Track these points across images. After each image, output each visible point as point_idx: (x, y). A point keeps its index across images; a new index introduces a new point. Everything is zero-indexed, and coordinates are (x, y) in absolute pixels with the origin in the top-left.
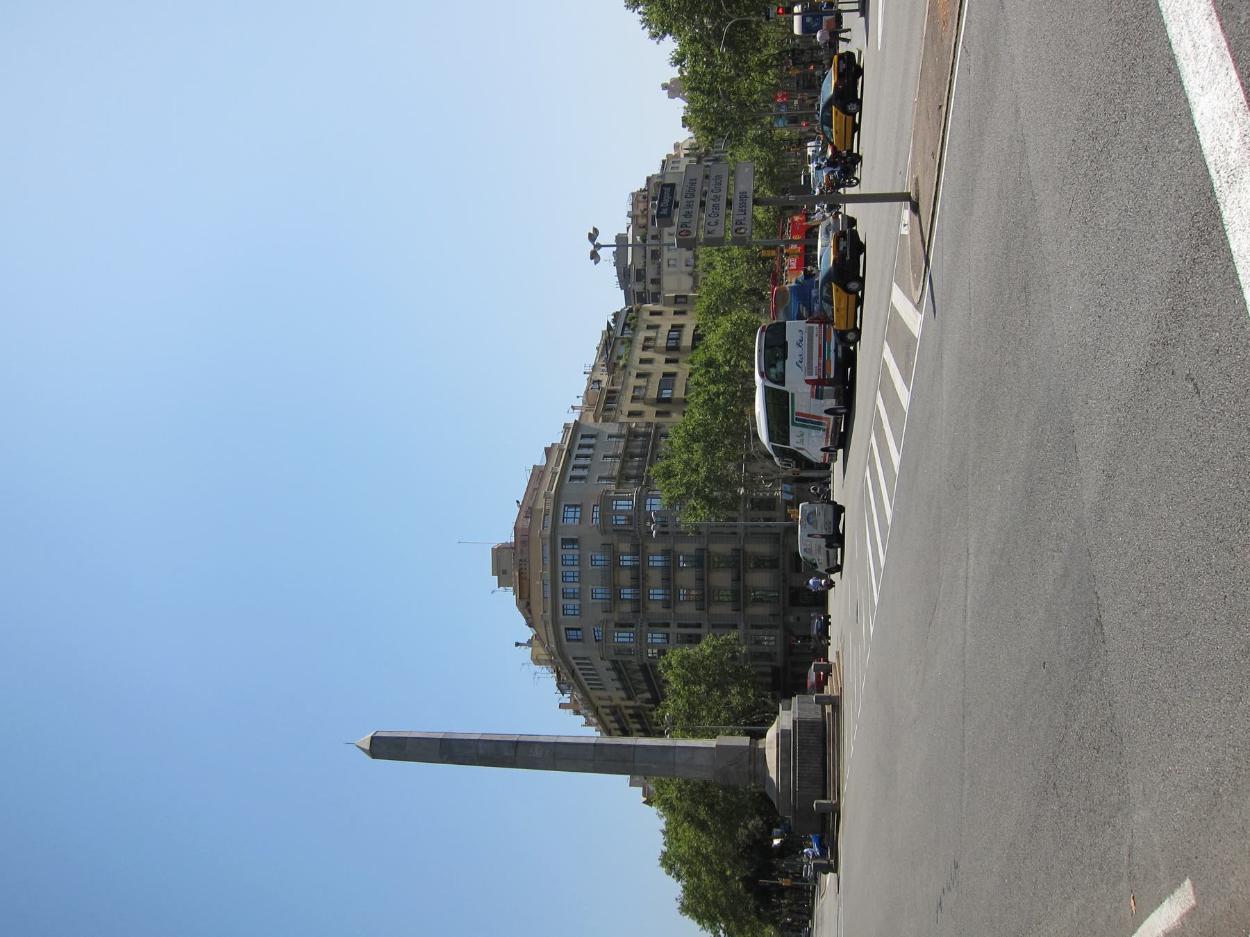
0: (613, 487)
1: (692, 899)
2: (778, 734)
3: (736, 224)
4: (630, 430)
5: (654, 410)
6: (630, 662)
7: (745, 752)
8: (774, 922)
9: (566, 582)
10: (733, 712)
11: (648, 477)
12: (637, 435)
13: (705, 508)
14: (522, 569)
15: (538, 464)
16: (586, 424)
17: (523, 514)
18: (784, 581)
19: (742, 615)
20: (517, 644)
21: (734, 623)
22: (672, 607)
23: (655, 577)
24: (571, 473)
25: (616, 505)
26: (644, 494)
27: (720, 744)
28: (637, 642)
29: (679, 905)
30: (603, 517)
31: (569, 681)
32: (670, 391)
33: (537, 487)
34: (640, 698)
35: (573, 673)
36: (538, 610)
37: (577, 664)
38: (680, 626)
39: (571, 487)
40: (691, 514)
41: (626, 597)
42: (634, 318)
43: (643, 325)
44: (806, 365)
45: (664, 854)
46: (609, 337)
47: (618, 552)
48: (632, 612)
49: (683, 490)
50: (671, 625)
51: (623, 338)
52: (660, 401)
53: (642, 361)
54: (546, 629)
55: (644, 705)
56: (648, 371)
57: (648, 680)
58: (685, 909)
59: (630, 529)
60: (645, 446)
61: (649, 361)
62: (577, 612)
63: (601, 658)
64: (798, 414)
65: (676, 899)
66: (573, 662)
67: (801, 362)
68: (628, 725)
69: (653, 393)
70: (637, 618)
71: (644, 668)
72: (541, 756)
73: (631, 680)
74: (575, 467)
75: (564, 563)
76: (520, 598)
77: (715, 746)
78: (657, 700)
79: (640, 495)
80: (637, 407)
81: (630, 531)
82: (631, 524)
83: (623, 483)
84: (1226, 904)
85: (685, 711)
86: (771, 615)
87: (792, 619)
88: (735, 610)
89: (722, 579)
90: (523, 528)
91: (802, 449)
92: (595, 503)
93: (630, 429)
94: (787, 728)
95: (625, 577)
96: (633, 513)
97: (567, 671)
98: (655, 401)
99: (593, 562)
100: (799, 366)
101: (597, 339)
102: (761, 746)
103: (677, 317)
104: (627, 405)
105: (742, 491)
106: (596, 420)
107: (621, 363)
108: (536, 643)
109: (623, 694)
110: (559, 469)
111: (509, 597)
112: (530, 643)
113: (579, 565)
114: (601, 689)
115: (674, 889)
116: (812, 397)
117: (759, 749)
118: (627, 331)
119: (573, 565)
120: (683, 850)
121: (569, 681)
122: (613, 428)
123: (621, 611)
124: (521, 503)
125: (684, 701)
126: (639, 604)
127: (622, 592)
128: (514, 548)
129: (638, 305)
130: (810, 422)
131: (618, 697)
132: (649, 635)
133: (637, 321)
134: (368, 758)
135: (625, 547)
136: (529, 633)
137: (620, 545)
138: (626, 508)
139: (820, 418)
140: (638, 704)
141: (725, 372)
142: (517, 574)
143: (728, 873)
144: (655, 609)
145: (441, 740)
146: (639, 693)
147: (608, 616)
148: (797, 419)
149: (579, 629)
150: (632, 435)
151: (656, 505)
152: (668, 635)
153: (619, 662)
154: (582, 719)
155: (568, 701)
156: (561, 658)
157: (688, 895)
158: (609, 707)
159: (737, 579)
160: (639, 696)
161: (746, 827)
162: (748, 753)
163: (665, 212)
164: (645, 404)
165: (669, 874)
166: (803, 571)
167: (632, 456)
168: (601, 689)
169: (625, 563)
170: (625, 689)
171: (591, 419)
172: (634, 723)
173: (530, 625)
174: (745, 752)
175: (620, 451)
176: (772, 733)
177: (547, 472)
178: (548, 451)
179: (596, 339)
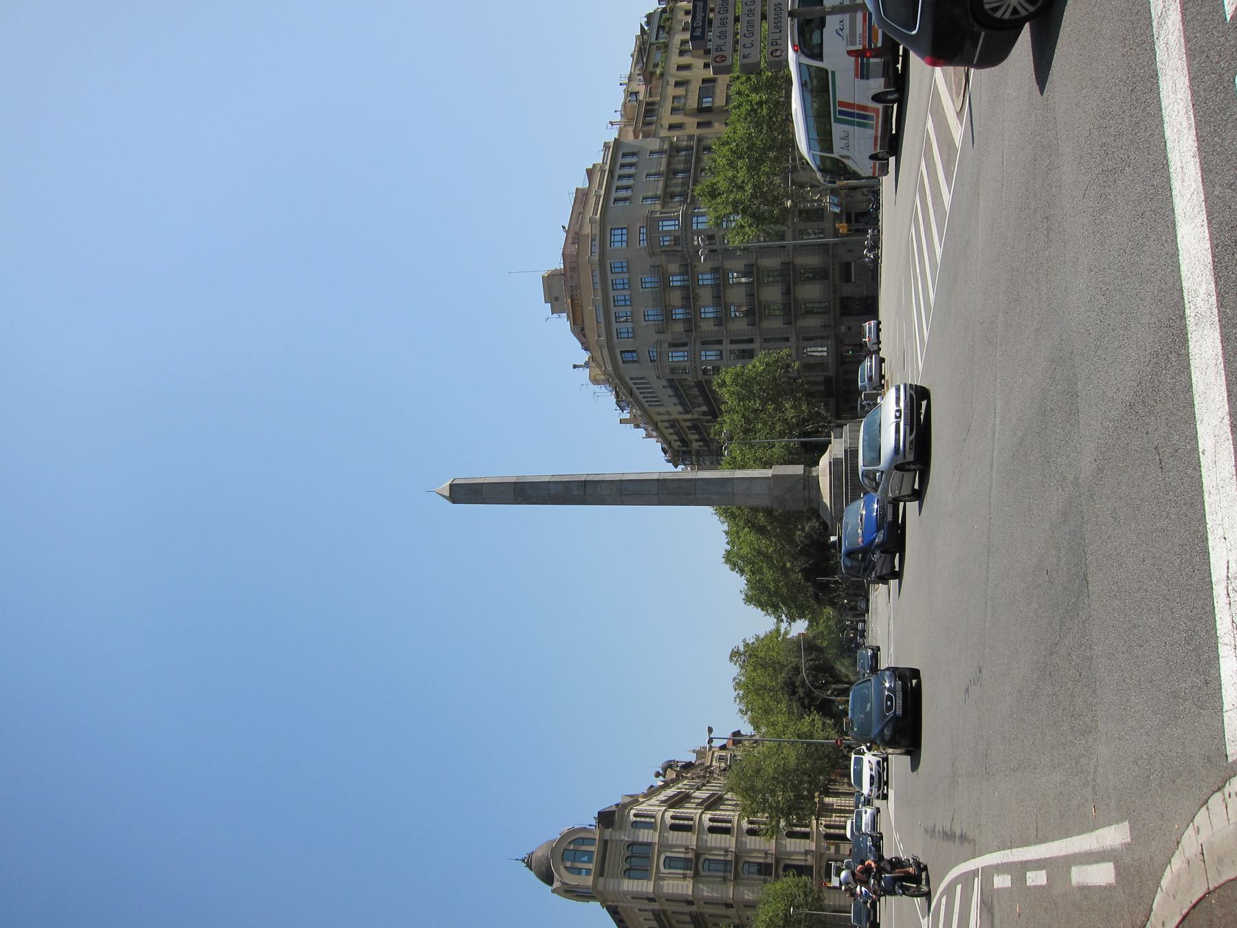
0: (658, 207)
1: (756, 590)
2: (830, 463)
3: (772, 45)
4: (671, 145)
5: (695, 121)
6: (686, 379)
7: (800, 480)
8: (833, 604)
9: (616, 289)
10: (788, 424)
11: (693, 196)
12: (679, 150)
13: (752, 226)
14: (573, 295)
15: (580, 187)
16: (626, 141)
17: (570, 241)
18: (834, 292)
19: (794, 328)
20: (575, 367)
21: (786, 336)
22: (724, 324)
23: (706, 296)
24: (614, 195)
25: (663, 226)
26: (689, 212)
27: (775, 473)
28: (691, 361)
29: (743, 596)
30: (650, 239)
31: (628, 400)
32: (710, 99)
33: (582, 211)
34: (696, 412)
35: (631, 393)
36: (592, 337)
37: (634, 384)
38: (732, 342)
39: (617, 210)
40: (738, 233)
41: (678, 317)
42: (668, 19)
43: (678, 27)
44: (848, 33)
45: (728, 552)
46: (643, 43)
47: (667, 273)
48: (685, 331)
49: (730, 209)
50: (724, 342)
51: (658, 43)
52: (701, 110)
53: (680, 68)
54: (602, 353)
55: (702, 417)
56: (688, 78)
58: (749, 599)
59: (677, 249)
60: (688, 161)
61: (687, 67)
62: (631, 335)
63: (657, 378)
64: (841, 104)
65: (741, 591)
66: (631, 383)
67: (842, 30)
68: (687, 436)
69: (693, 103)
70: (690, 337)
71: (699, 384)
72: (608, 493)
73: (687, 395)
74: (618, 188)
75: (615, 288)
76: (574, 324)
77: (770, 476)
78: (714, 413)
79: (686, 214)
80: (677, 119)
81: (677, 251)
82: (675, 244)
83: (668, 203)
85: (741, 425)
86: (822, 326)
87: (843, 329)
88: (787, 324)
89: (772, 294)
90: (570, 255)
91: (848, 158)
92: (642, 225)
93: (671, 144)
94: (839, 457)
95: (676, 298)
96: (679, 233)
97: (625, 391)
98: (696, 111)
99: (644, 285)
100: (839, 34)
101: (631, 46)
102: (814, 474)
104: (667, 118)
105: (789, 203)
106: (636, 136)
107: (658, 71)
108: (593, 364)
109: (680, 409)
110: (603, 192)
111: (563, 323)
112: (587, 365)
113: (631, 305)
114: (659, 405)
115: (739, 583)
116: (856, 76)
117: (812, 477)
118: (663, 34)
119: (622, 272)
120: (746, 550)
121: (628, 400)
122: (654, 144)
123: (674, 330)
124: (567, 229)
125: (740, 415)
126: (691, 323)
127: (673, 312)
128: (564, 275)
129: (671, 4)
130: (855, 115)
131: (676, 411)
132: (703, 353)
133: (671, 23)
134: (449, 503)
135: (674, 267)
136: (584, 356)
137: (669, 265)
138: (672, 228)
139: (865, 108)
140: (696, 416)
141: (767, 76)
142: (569, 301)
143: (788, 565)
144: (708, 327)
145: (515, 483)
146: (695, 407)
147: (662, 337)
148: (841, 113)
149: (634, 351)
150: (675, 149)
151: (704, 222)
152: (721, 351)
153: (676, 380)
154: (642, 432)
155: (628, 416)
156: (619, 379)
157: (752, 588)
158: (668, 421)
159: (788, 292)
160: (696, 409)
161: (803, 529)
162: (802, 481)
163: (698, 33)
164: (685, 115)
165: (733, 570)
166: (853, 280)
167: (676, 173)
168: (659, 405)
169: (675, 284)
170: (682, 404)
171: (631, 136)
172: (692, 434)
173: (586, 349)
174: (800, 480)
175: (663, 168)
176: (825, 461)
177: (591, 195)
178: (590, 173)
179: (630, 46)
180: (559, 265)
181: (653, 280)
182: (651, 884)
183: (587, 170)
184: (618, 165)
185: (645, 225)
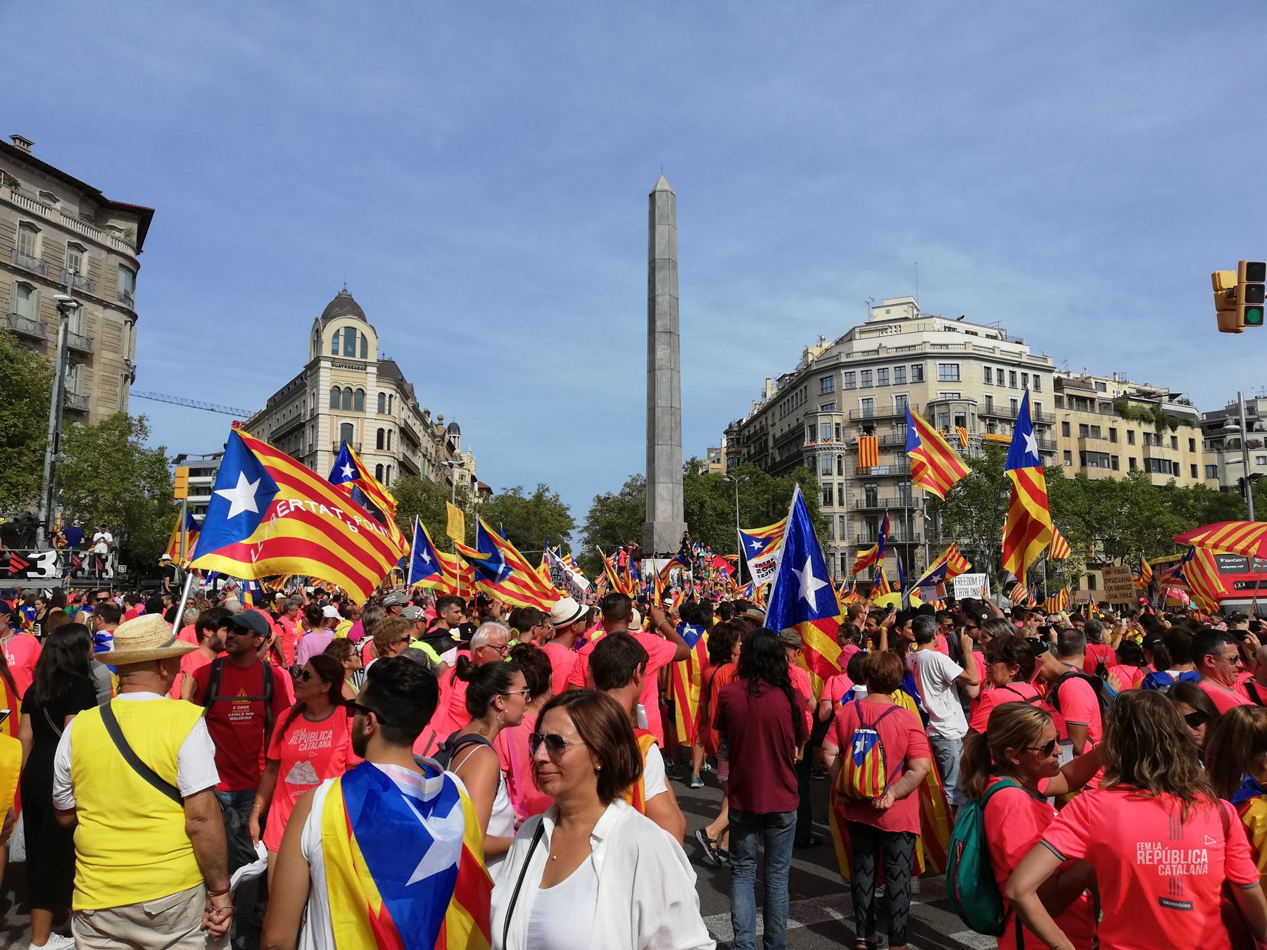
24: (994, 367)
50: (840, 477)
57: (790, 458)
84: (729, 580)
103: (1189, 468)
104: (1077, 418)
140: (771, 451)
179: (136, 377)
184: (1025, 371)
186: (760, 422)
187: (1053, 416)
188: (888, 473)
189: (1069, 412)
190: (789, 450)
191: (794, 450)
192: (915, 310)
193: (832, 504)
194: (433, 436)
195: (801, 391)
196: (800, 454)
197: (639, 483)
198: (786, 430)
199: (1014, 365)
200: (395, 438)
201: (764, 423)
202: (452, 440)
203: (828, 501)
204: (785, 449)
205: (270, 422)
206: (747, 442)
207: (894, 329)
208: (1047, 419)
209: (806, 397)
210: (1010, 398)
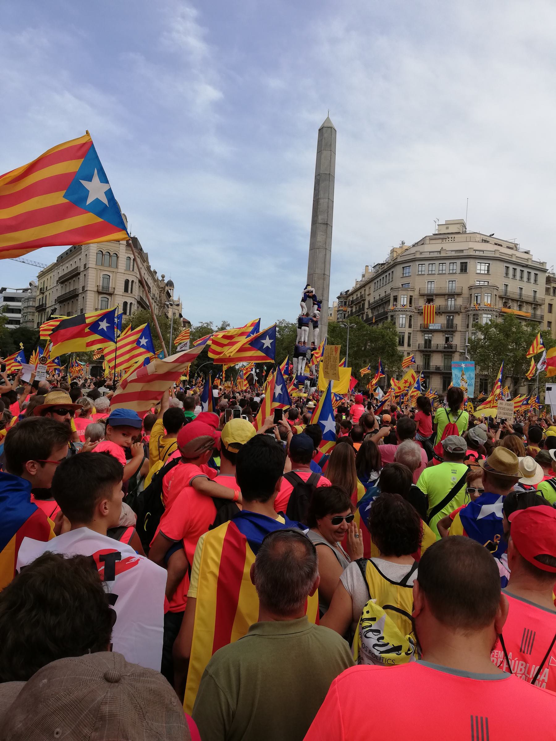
24: (511, 267)
50: (410, 329)
92: (489, 283)
132: (404, 316)
140: (366, 310)
180: (470, 229)
181: (453, 288)
182: (94, 266)
183: (529, 251)
184: (530, 271)
185: (489, 285)
186: (361, 293)
187: (544, 300)
188: (439, 328)
189: (553, 298)
190: (378, 310)
191: (381, 311)
192: (464, 228)
193: (403, 345)
194: (158, 286)
195: (389, 274)
196: (386, 313)
197: (283, 325)
198: (377, 298)
199: (523, 266)
200: (136, 286)
201: (363, 293)
202: (169, 291)
203: (401, 343)
204: (376, 309)
205: (59, 271)
206: (351, 304)
207: (450, 239)
208: (540, 302)
209: (392, 278)
210: (518, 287)
